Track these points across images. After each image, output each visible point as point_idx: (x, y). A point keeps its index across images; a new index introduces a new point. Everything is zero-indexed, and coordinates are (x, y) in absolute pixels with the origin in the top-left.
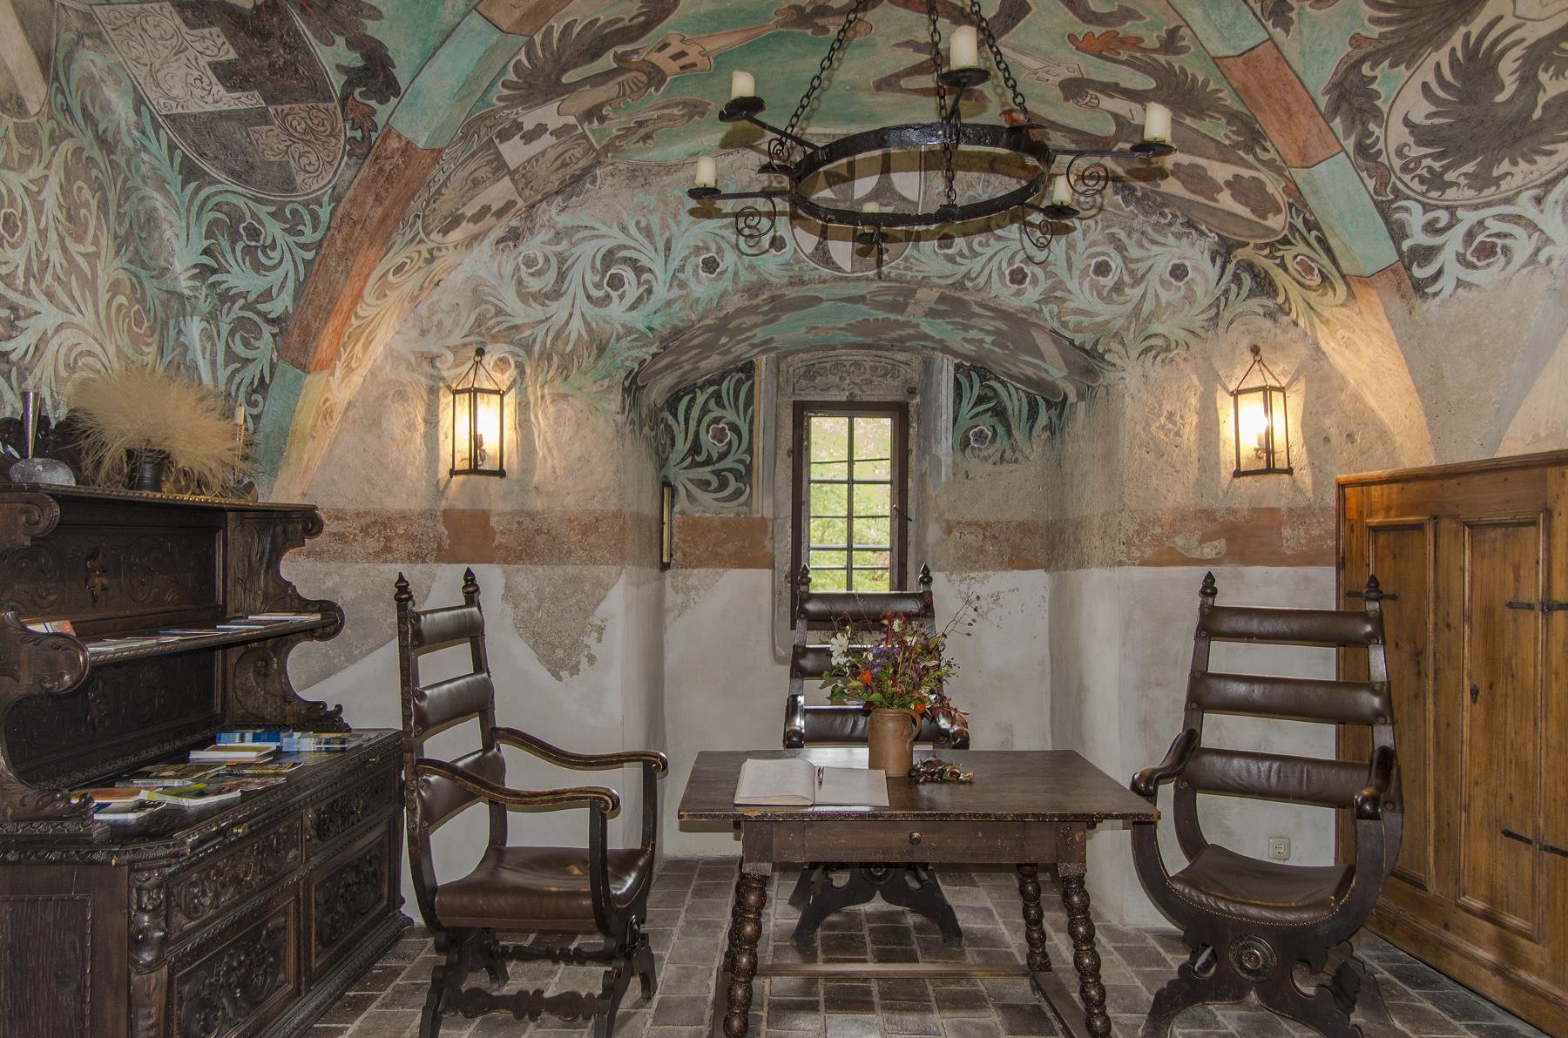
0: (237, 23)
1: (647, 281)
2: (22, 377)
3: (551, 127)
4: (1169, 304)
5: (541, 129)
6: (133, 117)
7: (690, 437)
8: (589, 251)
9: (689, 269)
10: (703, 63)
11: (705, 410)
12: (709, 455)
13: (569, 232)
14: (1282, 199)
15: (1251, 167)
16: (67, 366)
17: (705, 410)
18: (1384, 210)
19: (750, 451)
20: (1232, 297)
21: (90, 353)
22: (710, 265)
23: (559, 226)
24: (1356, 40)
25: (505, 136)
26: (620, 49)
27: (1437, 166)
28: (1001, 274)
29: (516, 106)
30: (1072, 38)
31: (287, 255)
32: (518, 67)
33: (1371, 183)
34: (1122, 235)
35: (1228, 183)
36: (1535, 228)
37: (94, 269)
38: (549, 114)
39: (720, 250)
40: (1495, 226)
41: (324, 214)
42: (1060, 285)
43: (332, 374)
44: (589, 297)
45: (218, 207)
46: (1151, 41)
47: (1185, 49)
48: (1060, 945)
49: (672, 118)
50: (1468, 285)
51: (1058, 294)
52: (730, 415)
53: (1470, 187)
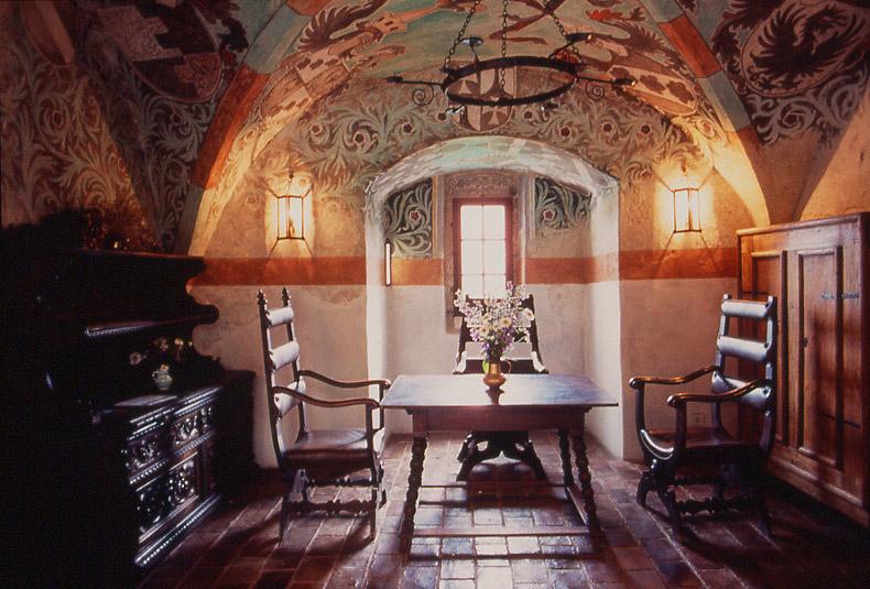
0: (165, 14)
1: (376, 138)
2: (65, 195)
3: (325, 61)
4: (641, 146)
5: (320, 62)
6: (117, 63)
7: (400, 217)
8: (347, 123)
9: (397, 130)
10: (402, 28)
11: (407, 204)
12: (410, 228)
13: (336, 113)
14: (694, 93)
15: (678, 77)
16: (87, 190)
17: (407, 204)
18: (743, 98)
19: (431, 224)
20: (672, 142)
21: (98, 183)
22: (408, 129)
23: (331, 111)
24: (726, 15)
25: (302, 66)
26: (359, 21)
27: (767, 77)
28: (557, 131)
29: (307, 51)
30: (588, 13)
31: (194, 130)
32: (308, 32)
33: (736, 86)
34: (617, 111)
35: (668, 86)
36: (815, 108)
37: (99, 140)
38: (324, 54)
39: (412, 121)
40: (798, 107)
41: (212, 108)
42: (586, 137)
43: (217, 189)
44: (346, 147)
45: (160, 107)
46: (626, 14)
47: (643, 19)
48: (575, 470)
49: (388, 55)
50: (784, 137)
51: (586, 141)
52: (421, 207)
53: (783, 87)
